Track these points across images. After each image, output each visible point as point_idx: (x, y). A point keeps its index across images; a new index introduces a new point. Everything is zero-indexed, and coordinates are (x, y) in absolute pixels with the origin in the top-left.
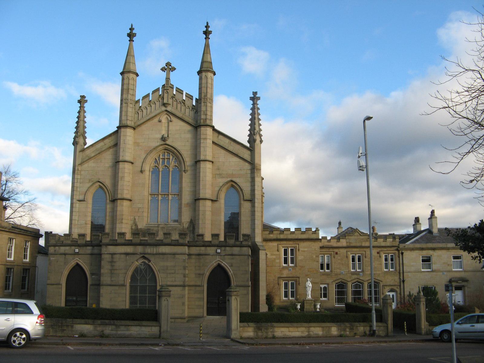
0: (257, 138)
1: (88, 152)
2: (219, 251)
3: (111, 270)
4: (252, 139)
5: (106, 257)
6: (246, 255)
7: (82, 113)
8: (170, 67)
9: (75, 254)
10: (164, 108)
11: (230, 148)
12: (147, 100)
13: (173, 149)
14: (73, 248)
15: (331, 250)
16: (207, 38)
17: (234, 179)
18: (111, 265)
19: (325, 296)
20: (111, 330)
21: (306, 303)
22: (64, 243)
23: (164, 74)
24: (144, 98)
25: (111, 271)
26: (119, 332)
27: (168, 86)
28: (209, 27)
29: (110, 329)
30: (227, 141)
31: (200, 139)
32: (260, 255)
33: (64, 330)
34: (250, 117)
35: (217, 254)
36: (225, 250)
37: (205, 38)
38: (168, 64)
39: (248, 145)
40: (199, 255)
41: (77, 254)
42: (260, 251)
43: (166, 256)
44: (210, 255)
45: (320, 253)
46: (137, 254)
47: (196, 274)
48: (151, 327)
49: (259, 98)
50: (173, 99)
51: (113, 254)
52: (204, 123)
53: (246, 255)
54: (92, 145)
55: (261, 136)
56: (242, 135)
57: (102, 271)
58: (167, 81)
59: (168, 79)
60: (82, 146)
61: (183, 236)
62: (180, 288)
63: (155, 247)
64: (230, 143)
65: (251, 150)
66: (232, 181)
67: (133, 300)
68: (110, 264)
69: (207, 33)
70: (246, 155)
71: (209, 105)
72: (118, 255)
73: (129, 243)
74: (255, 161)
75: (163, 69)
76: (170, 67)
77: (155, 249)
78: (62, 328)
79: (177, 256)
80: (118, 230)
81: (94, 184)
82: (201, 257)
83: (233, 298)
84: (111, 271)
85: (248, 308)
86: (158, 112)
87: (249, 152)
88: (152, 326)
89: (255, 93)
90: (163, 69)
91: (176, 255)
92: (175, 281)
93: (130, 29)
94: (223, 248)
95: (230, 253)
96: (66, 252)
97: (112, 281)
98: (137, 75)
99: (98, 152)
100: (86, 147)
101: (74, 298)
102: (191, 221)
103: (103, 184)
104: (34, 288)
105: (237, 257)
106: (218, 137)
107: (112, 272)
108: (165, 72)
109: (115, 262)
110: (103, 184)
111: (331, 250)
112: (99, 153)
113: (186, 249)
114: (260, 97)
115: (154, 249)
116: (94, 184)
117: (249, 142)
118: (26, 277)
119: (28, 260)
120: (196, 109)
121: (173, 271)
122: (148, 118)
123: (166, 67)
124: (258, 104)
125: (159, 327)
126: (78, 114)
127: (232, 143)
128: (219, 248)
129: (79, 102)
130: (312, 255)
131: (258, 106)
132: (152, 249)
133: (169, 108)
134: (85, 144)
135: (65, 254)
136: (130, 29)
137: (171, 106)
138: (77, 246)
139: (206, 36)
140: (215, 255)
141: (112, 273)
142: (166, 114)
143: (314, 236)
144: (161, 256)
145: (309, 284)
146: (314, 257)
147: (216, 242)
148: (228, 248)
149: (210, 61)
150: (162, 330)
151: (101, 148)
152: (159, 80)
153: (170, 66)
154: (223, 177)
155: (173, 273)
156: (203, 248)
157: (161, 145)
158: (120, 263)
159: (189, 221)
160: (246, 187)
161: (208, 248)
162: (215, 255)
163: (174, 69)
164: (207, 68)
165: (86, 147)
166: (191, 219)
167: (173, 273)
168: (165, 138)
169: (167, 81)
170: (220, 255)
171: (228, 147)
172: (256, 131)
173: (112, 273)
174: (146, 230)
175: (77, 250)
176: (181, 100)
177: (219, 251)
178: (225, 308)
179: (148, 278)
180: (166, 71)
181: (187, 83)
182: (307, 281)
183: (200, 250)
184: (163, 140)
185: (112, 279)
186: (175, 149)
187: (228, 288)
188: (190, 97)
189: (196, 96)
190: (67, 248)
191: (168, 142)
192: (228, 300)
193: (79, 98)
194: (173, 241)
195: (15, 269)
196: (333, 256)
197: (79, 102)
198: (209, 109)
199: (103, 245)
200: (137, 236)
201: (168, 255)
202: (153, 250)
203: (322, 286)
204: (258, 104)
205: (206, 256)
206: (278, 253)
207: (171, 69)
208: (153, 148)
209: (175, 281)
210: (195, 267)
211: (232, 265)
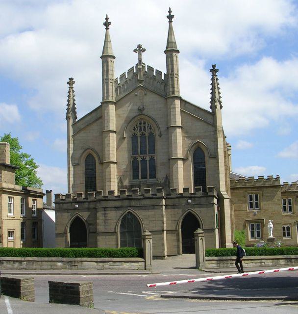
0: (217, 104)
1: (78, 124)
4: (213, 107)
7: (71, 93)
8: (141, 49)
16: (170, 22)
18: (105, 217)
19: (289, 235)
23: (137, 54)
28: (171, 12)
31: (170, 108)
32: (225, 203)
34: (211, 86)
36: (194, 200)
38: (139, 46)
39: (211, 111)
42: (225, 200)
47: (172, 221)
49: (217, 70)
52: (115, 233)
54: (82, 119)
55: (220, 102)
56: (206, 105)
57: (98, 221)
59: (140, 60)
70: (210, 119)
71: (175, 79)
73: (118, 199)
74: (217, 124)
75: (135, 51)
77: (101, 221)
80: (108, 190)
81: (85, 151)
83: (200, 238)
90: (135, 51)
93: (106, 19)
94: (193, 199)
97: (106, 229)
98: (114, 57)
100: (76, 120)
104: (42, 237)
112: (88, 125)
116: (85, 151)
117: (211, 108)
118: (35, 229)
119: (36, 215)
120: (165, 83)
121: (154, 219)
123: (138, 49)
125: (144, 263)
126: (68, 94)
129: (68, 83)
131: (217, 77)
134: (76, 118)
136: (106, 19)
143: (276, 184)
145: (271, 225)
147: (186, 194)
152: (133, 62)
159: (165, 177)
163: (144, 50)
164: (172, 47)
165: (76, 120)
166: (167, 176)
172: (216, 99)
173: (105, 223)
178: (194, 247)
181: (157, 62)
182: (269, 222)
187: (195, 231)
188: (159, 73)
189: (164, 71)
192: (196, 240)
193: (68, 81)
195: (27, 223)
197: (68, 83)
198: (176, 82)
203: (286, 226)
206: (245, 199)
207: (141, 50)
208: (131, 118)
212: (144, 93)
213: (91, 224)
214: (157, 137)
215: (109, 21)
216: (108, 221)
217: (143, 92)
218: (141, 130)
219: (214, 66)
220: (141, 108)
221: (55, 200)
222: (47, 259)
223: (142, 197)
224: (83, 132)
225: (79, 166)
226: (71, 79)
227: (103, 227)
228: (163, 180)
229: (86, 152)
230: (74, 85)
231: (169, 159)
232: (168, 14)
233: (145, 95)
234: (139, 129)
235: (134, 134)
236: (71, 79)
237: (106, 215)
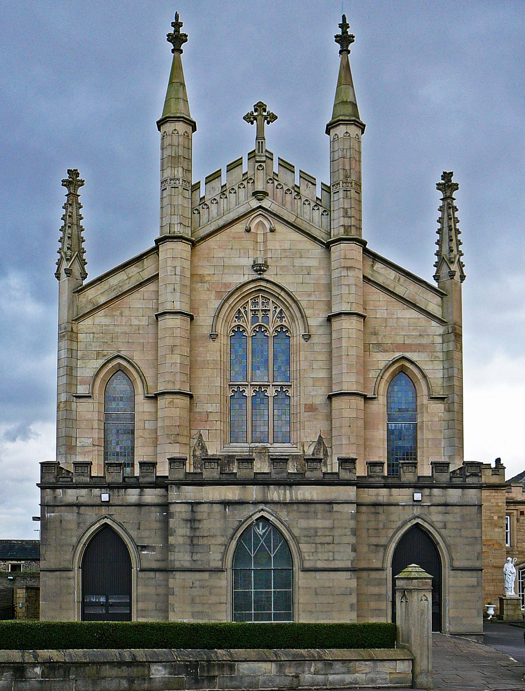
2: (418, 496)
3: (192, 537)
5: (180, 511)
6: (475, 505)
8: (265, 114)
9: (101, 506)
10: (254, 204)
11: (399, 290)
12: (217, 185)
13: (278, 291)
14: (96, 491)
15: (513, 508)
17: (408, 355)
18: (191, 528)
20: (314, 674)
21: (507, 604)
22: (74, 481)
24: (210, 179)
25: (192, 541)
26: (331, 677)
27: (262, 154)
29: (312, 670)
30: (392, 274)
33: (214, 677)
35: (415, 503)
37: (341, 52)
38: (260, 107)
40: (375, 505)
41: (107, 504)
43: (312, 508)
44: (399, 505)
45: (507, 513)
46: (248, 503)
48: (394, 662)
49: (455, 187)
50: (273, 183)
51: (194, 504)
53: (475, 505)
58: (259, 142)
59: (260, 138)
60: (77, 279)
61: (349, 466)
62: (345, 573)
63: (287, 487)
64: (399, 281)
65: (443, 294)
66: (404, 358)
67: (240, 603)
68: (189, 526)
69: (344, 40)
72: (207, 505)
76: (265, 114)
77: (181, 540)
78: (208, 671)
79: (336, 507)
82: (380, 509)
84: (192, 541)
85: (143, 612)
86: (242, 210)
87: (438, 299)
88: (396, 660)
89: (447, 176)
91: (334, 505)
92: (334, 560)
94: (427, 491)
95: (442, 500)
96: (81, 500)
99: (113, 295)
101: (103, 599)
102: (319, 439)
103: (129, 362)
105: (457, 509)
106: (373, 266)
107: (193, 542)
108: (252, 123)
109: (199, 521)
110: (129, 362)
111: (513, 508)
113: (350, 492)
114: (458, 185)
115: (285, 491)
116: (109, 361)
121: (328, 539)
122: (221, 223)
124: (454, 199)
127: (403, 278)
128: (417, 490)
129: (66, 183)
130: (492, 515)
132: (282, 492)
133: (266, 203)
134: (84, 276)
135: (78, 506)
137: (269, 198)
138: (104, 488)
139: (342, 46)
140: (409, 505)
141: (194, 545)
142: (260, 214)
144: (303, 508)
146: (496, 518)
148: (436, 491)
149: (353, 100)
150: (418, 670)
151: (120, 284)
153: (265, 111)
154: (385, 351)
155: (328, 544)
156: (384, 491)
157: (253, 281)
158: (213, 523)
160: (435, 372)
161: (395, 491)
162: (409, 505)
163: (273, 118)
165: (85, 282)
167: (328, 544)
168: (260, 267)
169: (259, 142)
170: (421, 505)
171: (394, 288)
173: (192, 544)
174: (225, 457)
175: (105, 497)
176: (290, 186)
177: (418, 496)
179: (272, 556)
180: (255, 121)
183: (378, 495)
184: (256, 271)
185: (195, 558)
186: (282, 289)
190: (84, 492)
191: (266, 276)
193: (66, 177)
194: (326, 475)
196: (515, 518)
197: (66, 183)
199: (172, 484)
200: (245, 464)
201: (317, 505)
202: (285, 494)
204: (454, 199)
205: (392, 508)
207: (266, 118)
209: (334, 560)
210: (368, 529)
211: (445, 526)
212: (268, 226)
213: (144, 548)
214: (297, 340)
215: (182, 31)
216: (201, 541)
217: (265, 222)
218: (255, 318)
219: (447, 176)
220: (260, 261)
221: (42, 478)
222: (114, 653)
223: (298, 478)
224: (101, 313)
225: (90, 400)
226: (73, 173)
227: (188, 557)
228: (312, 449)
229: (110, 365)
230: (80, 191)
231: (330, 397)
232: (339, 32)
233: (272, 231)
234: (250, 315)
235: (239, 327)
236: (73, 173)
237: (197, 525)
